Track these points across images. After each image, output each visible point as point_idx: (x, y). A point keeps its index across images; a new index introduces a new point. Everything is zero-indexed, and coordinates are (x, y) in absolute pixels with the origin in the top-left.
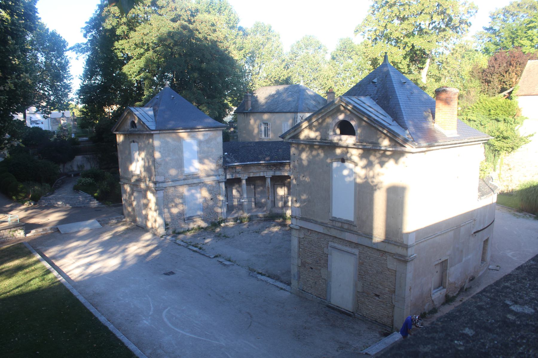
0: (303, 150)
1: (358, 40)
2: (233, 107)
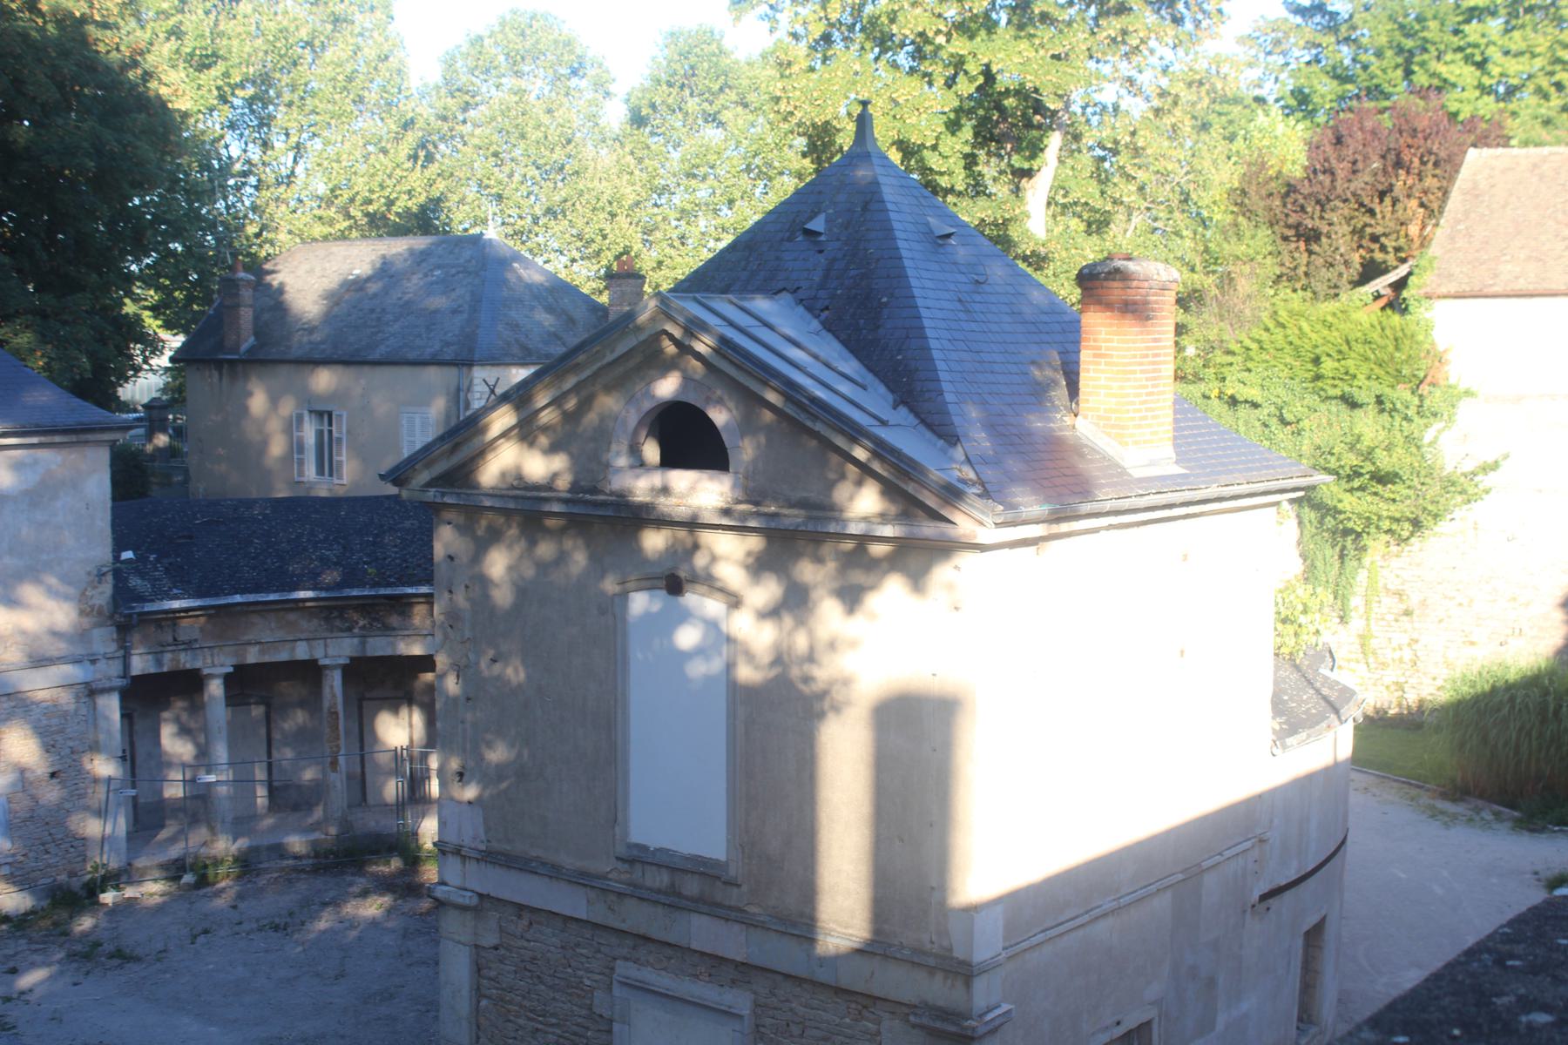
0: (495, 536)
1: (748, 41)
2: (164, 334)
